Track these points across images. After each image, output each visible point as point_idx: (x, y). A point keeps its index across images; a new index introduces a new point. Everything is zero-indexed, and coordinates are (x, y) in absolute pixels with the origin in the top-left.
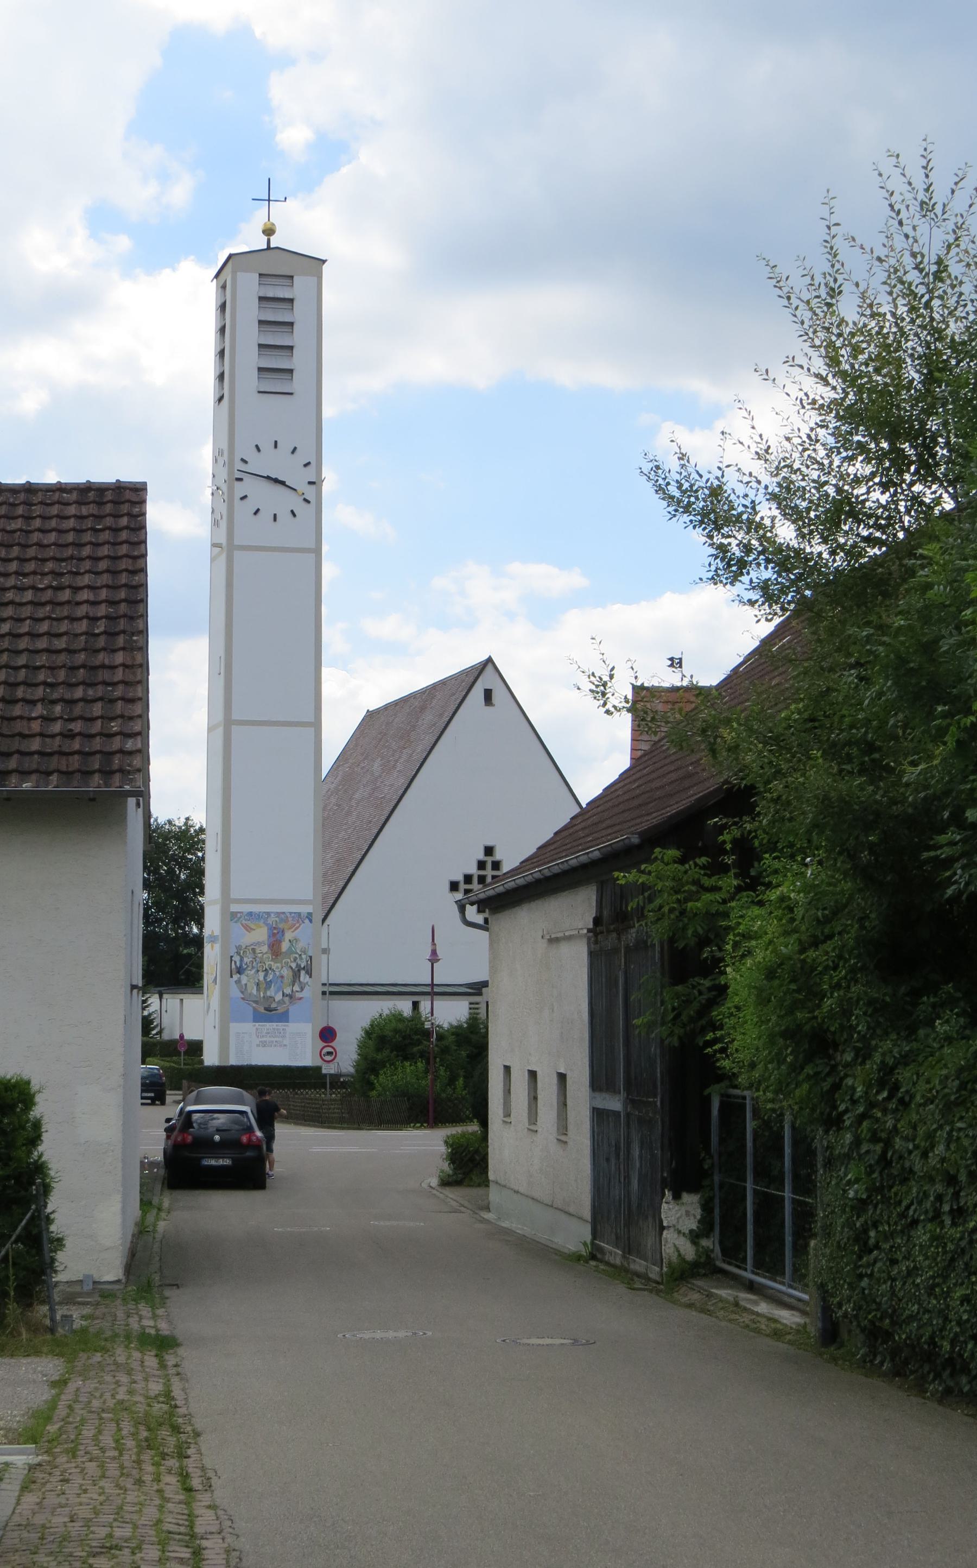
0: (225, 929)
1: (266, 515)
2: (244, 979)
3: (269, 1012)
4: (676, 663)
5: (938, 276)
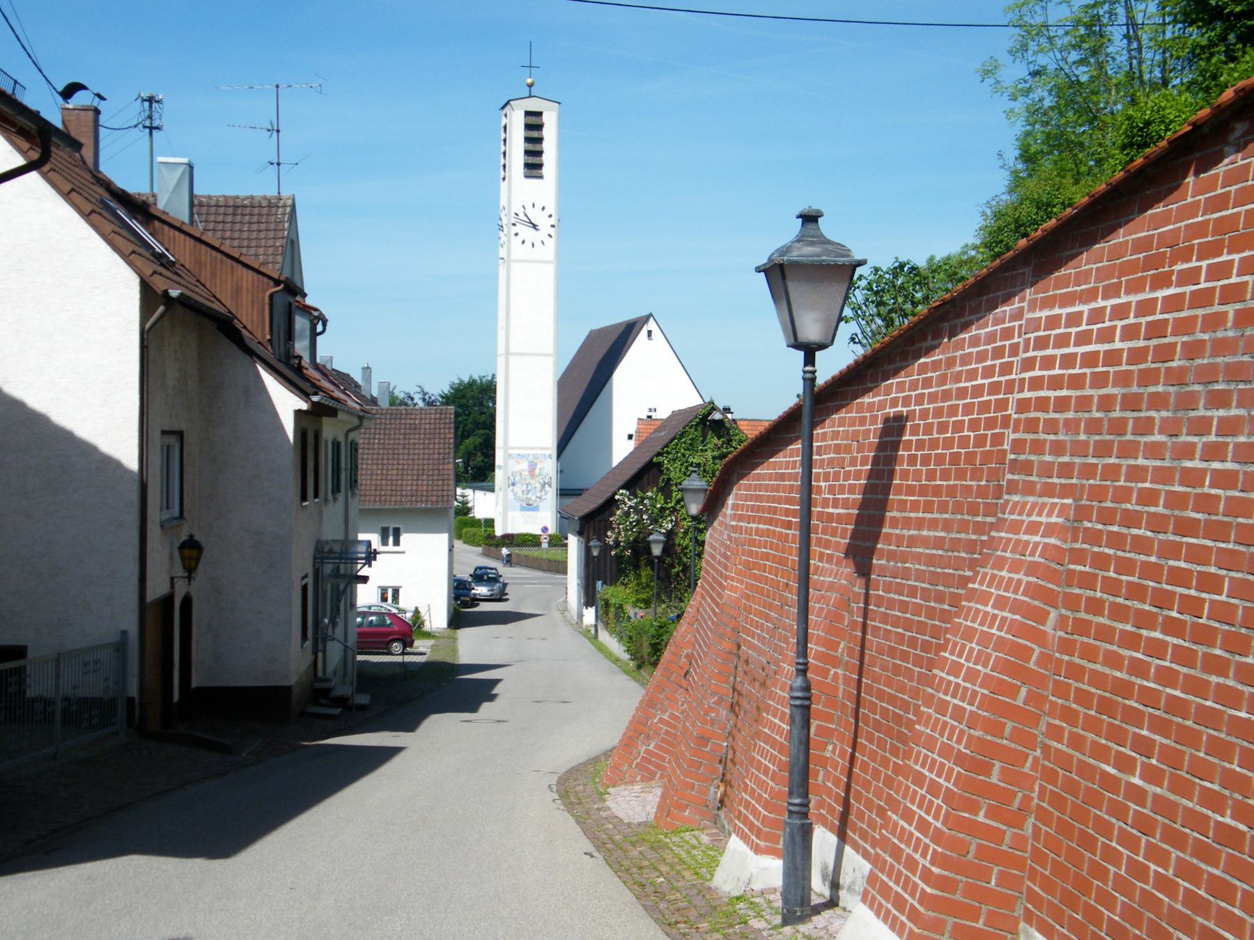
0: (506, 463)
1: (528, 244)
2: (515, 488)
3: (529, 507)
4: (630, 437)
5: (1131, 145)
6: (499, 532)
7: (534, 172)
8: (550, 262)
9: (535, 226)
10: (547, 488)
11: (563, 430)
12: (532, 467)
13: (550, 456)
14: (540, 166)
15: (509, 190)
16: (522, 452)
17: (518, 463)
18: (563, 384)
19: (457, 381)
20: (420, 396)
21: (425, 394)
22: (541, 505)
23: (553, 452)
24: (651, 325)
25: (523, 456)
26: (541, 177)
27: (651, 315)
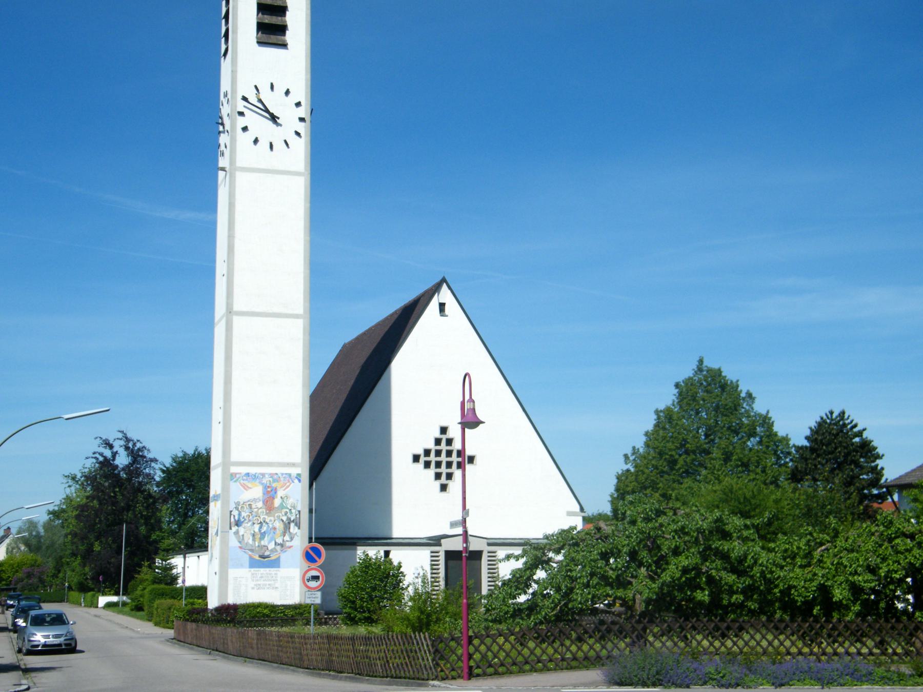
0: (226, 488)
1: (264, 144)
2: (242, 530)
3: (264, 560)
6: (213, 602)
7: (273, 38)
8: (296, 316)
9: (274, 118)
10: (293, 529)
11: (318, 448)
12: (270, 495)
13: (299, 477)
14: (282, 29)
15: (234, 72)
16: (253, 470)
17: (246, 488)
18: (317, 400)
19: (180, 454)
20: (122, 443)
21: (128, 440)
22: (284, 557)
23: (303, 470)
24: (445, 295)
25: (254, 477)
26: (284, 45)
27: (444, 280)
